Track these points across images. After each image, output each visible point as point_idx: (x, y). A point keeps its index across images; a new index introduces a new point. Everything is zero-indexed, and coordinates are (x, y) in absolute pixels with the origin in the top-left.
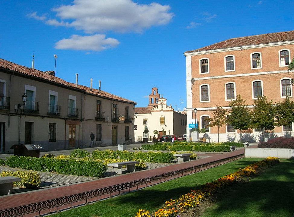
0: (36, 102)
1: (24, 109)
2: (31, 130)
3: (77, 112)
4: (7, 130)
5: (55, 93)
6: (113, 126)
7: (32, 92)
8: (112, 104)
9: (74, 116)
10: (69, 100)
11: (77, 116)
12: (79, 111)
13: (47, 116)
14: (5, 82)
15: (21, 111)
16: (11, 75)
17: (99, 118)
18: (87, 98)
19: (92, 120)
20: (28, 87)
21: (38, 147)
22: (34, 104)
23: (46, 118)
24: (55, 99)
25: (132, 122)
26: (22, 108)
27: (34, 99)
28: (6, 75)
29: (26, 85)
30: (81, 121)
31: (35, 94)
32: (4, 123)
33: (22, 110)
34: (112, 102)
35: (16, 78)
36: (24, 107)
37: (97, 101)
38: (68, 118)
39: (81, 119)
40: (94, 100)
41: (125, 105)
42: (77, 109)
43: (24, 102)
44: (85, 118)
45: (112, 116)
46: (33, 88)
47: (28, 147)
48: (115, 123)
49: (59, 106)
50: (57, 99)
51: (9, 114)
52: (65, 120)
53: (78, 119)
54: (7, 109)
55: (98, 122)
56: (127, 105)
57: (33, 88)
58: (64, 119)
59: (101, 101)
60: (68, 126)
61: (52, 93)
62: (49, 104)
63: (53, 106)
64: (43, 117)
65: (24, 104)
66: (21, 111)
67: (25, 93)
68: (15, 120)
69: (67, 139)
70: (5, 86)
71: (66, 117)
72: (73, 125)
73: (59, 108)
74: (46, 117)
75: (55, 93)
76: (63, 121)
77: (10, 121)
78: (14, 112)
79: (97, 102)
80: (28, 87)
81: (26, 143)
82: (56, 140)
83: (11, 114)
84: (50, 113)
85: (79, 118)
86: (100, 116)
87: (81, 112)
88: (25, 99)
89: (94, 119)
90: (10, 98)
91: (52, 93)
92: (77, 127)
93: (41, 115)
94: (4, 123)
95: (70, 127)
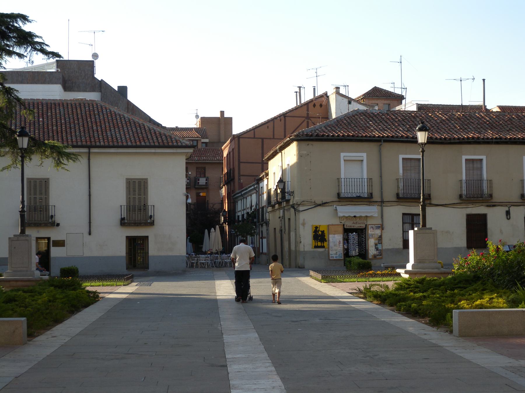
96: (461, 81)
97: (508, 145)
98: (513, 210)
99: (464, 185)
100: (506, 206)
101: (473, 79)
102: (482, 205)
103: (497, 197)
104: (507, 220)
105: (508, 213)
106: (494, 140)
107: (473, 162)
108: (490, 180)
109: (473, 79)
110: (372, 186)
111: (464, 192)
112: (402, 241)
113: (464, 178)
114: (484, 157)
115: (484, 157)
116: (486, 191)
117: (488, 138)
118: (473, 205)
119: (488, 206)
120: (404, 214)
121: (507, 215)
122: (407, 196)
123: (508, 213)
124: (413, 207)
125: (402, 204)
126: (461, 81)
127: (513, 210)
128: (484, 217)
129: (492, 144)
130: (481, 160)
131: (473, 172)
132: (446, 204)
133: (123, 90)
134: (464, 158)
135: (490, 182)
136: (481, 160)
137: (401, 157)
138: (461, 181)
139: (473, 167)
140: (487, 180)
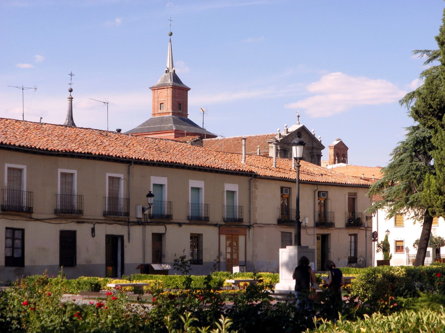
0: (239, 206)
1: (149, 215)
2: (161, 245)
3: (241, 212)
4: (126, 247)
5: (199, 184)
6: (317, 234)
7: (161, 186)
8: (315, 191)
9: (236, 219)
10: (225, 193)
11: (241, 220)
12: (246, 211)
13: (187, 221)
14: (122, 176)
15: (145, 217)
16: (129, 166)
17: (427, 240)
18: (261, 185)
19: (272, 225)
20: (155, 180)
21: (167, 267)
22: (166, 205)
23: (184, 227)
24: (200, 192)
25: (366, 226)
26: (147, 212)
27: (166, 197)
28: (123, 167)
29: (152, 177)
30: (249, 227)
31: (166, 188)
32: (122, 237)
33: (148, 217)
34: (315, 187)
35: (136, 169)
36: (150, 211)
37: (282, 188)
38: (223, 223)
39: (248, 224)
40: (276, 188)
41: (347, 191)
42: (240, 207)
43: (149, 204)
44: (258, 222)
45: (314, 216)
46: (163, 180)
47: (156, 267)
48: (321, 228)
49: (207, 205)
50: (203, 193)
51: (128, 223)
52: (219, 228)
53: (244, 224)
54: (126, 216)
55: (284, 228)
56: (352, 190)
57: (163, 180)
58: (216, 225)
59: (290, 188)
60: (223, 237)
61: (193, 183)
62: (225, 204)
63: (231, 207)
64: (180, 224)
65: (150, 207)
66: (145, 217)
67: (151, 190)
68: (136, 231)
69: (222, 260)
70: (122, 183)
71: (220, 223)
72: (234, 235)
73: (241, 209)
74: (185, 224)
75: (199, 184)
76: (216, 230)
77: (131, 233)
78: (135, 220)
79: (282, 191)
80: (155, 180)
81: (154, 262)
82: (203, 261)
83: (132, 224)
84: (192, 217)
85: (246, 222)
86: (289, 217)
87: (250, 211)
88: (151, 200)
89: (276, 222)
90: (129, 199)
91: (193, 183)
92: (241, 239)
93: (176, 221)
94: (122, 237)
95: (227, 239)
96: (23, 89)
97: (45, 156)
98: (97, 227)
99: (59, 199)
100: (92, 223)
101: (35, 89)
102: (73, 222)
103: (88, 213)
104: (92, 238)
105: (93, 230)
106: (87, 155)
107: (66, 175)
108: (80, 196)
109: (35, 89)
110: (241, 212)
111: (59, 207)
112: (4, 258)
113: (59, 192)
114: (75, 172)
115: (75, 172)
116: (25, 204)
117: (91, 153)
118: (66, 221)
119: (78, 222)
120: (7, 228)
121: (92, 233)
122: (302, 227)
123: (93, 230)
124: (15, 221)
125: (6, 217)
126: (23, 89)
127: (97, 227)
128: (73, 234)
129: (85, 159)
130: (21, 170)
131: (65, 187)
132: (44, 219)
133: (188, 114)
134: (7, 165)
135: (80, 197)
136: (72, 175)
137: (7, 165)
138: (188, 203)
139: (66, 182)
140: (27, 192)
